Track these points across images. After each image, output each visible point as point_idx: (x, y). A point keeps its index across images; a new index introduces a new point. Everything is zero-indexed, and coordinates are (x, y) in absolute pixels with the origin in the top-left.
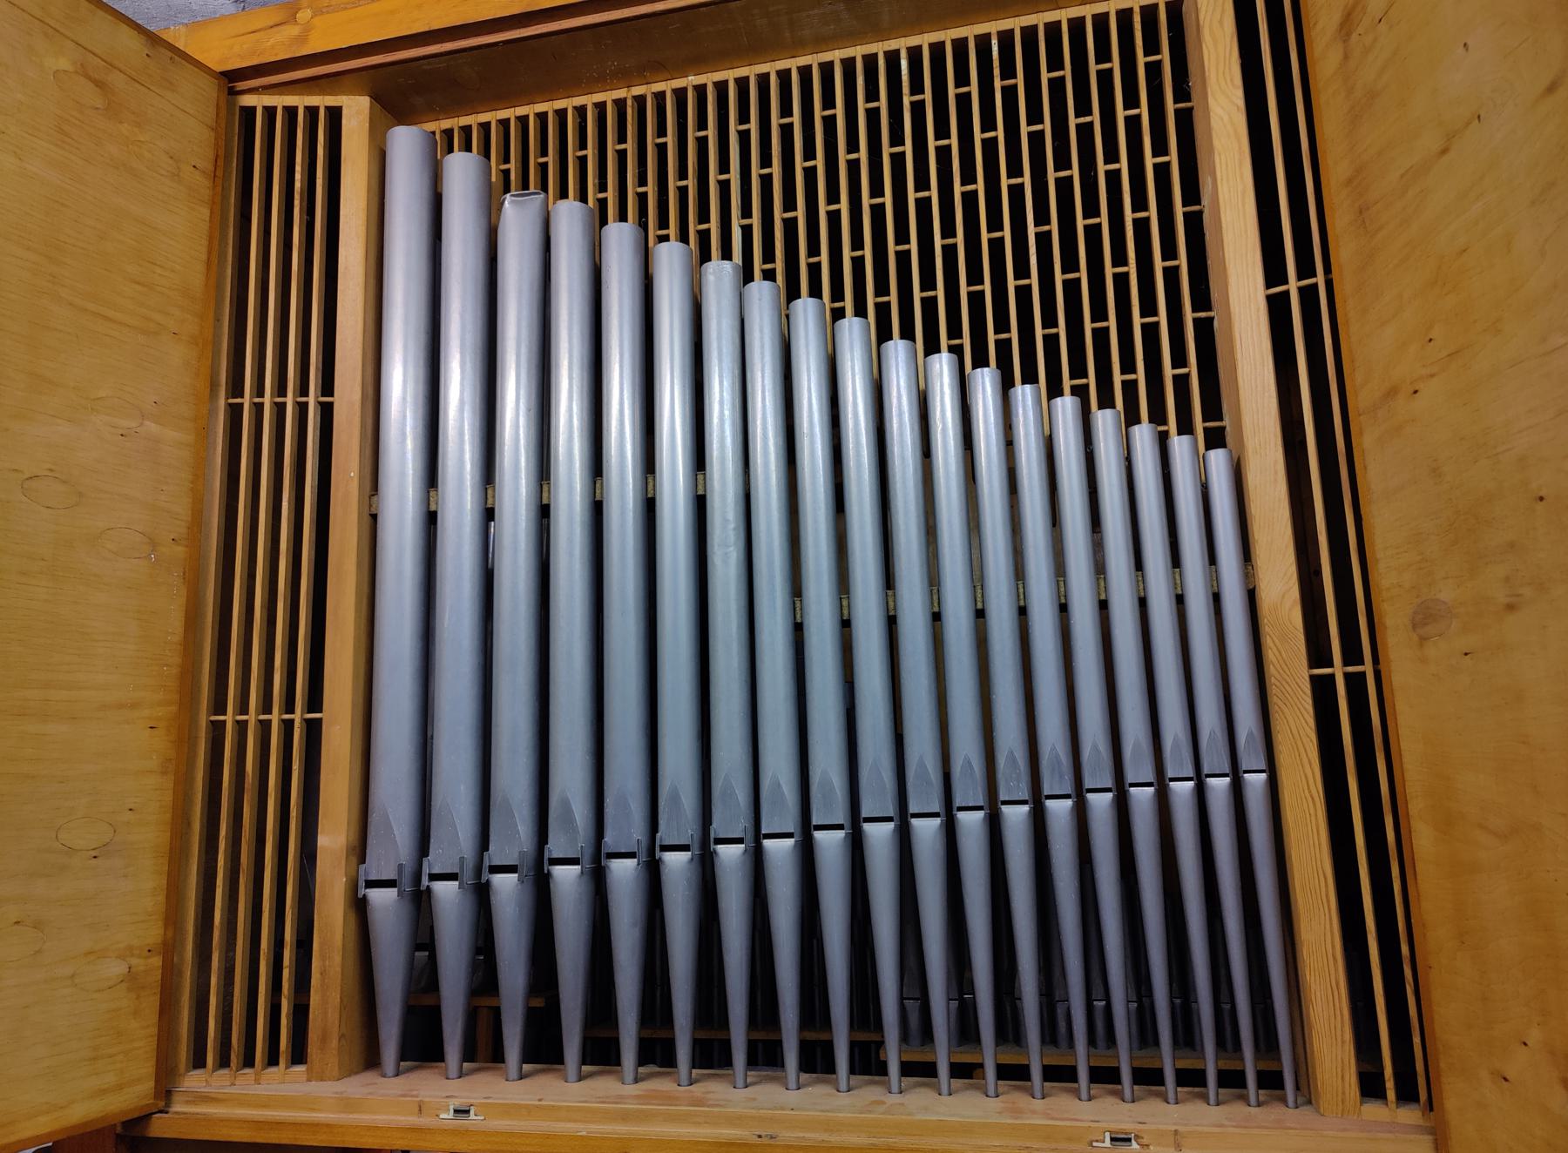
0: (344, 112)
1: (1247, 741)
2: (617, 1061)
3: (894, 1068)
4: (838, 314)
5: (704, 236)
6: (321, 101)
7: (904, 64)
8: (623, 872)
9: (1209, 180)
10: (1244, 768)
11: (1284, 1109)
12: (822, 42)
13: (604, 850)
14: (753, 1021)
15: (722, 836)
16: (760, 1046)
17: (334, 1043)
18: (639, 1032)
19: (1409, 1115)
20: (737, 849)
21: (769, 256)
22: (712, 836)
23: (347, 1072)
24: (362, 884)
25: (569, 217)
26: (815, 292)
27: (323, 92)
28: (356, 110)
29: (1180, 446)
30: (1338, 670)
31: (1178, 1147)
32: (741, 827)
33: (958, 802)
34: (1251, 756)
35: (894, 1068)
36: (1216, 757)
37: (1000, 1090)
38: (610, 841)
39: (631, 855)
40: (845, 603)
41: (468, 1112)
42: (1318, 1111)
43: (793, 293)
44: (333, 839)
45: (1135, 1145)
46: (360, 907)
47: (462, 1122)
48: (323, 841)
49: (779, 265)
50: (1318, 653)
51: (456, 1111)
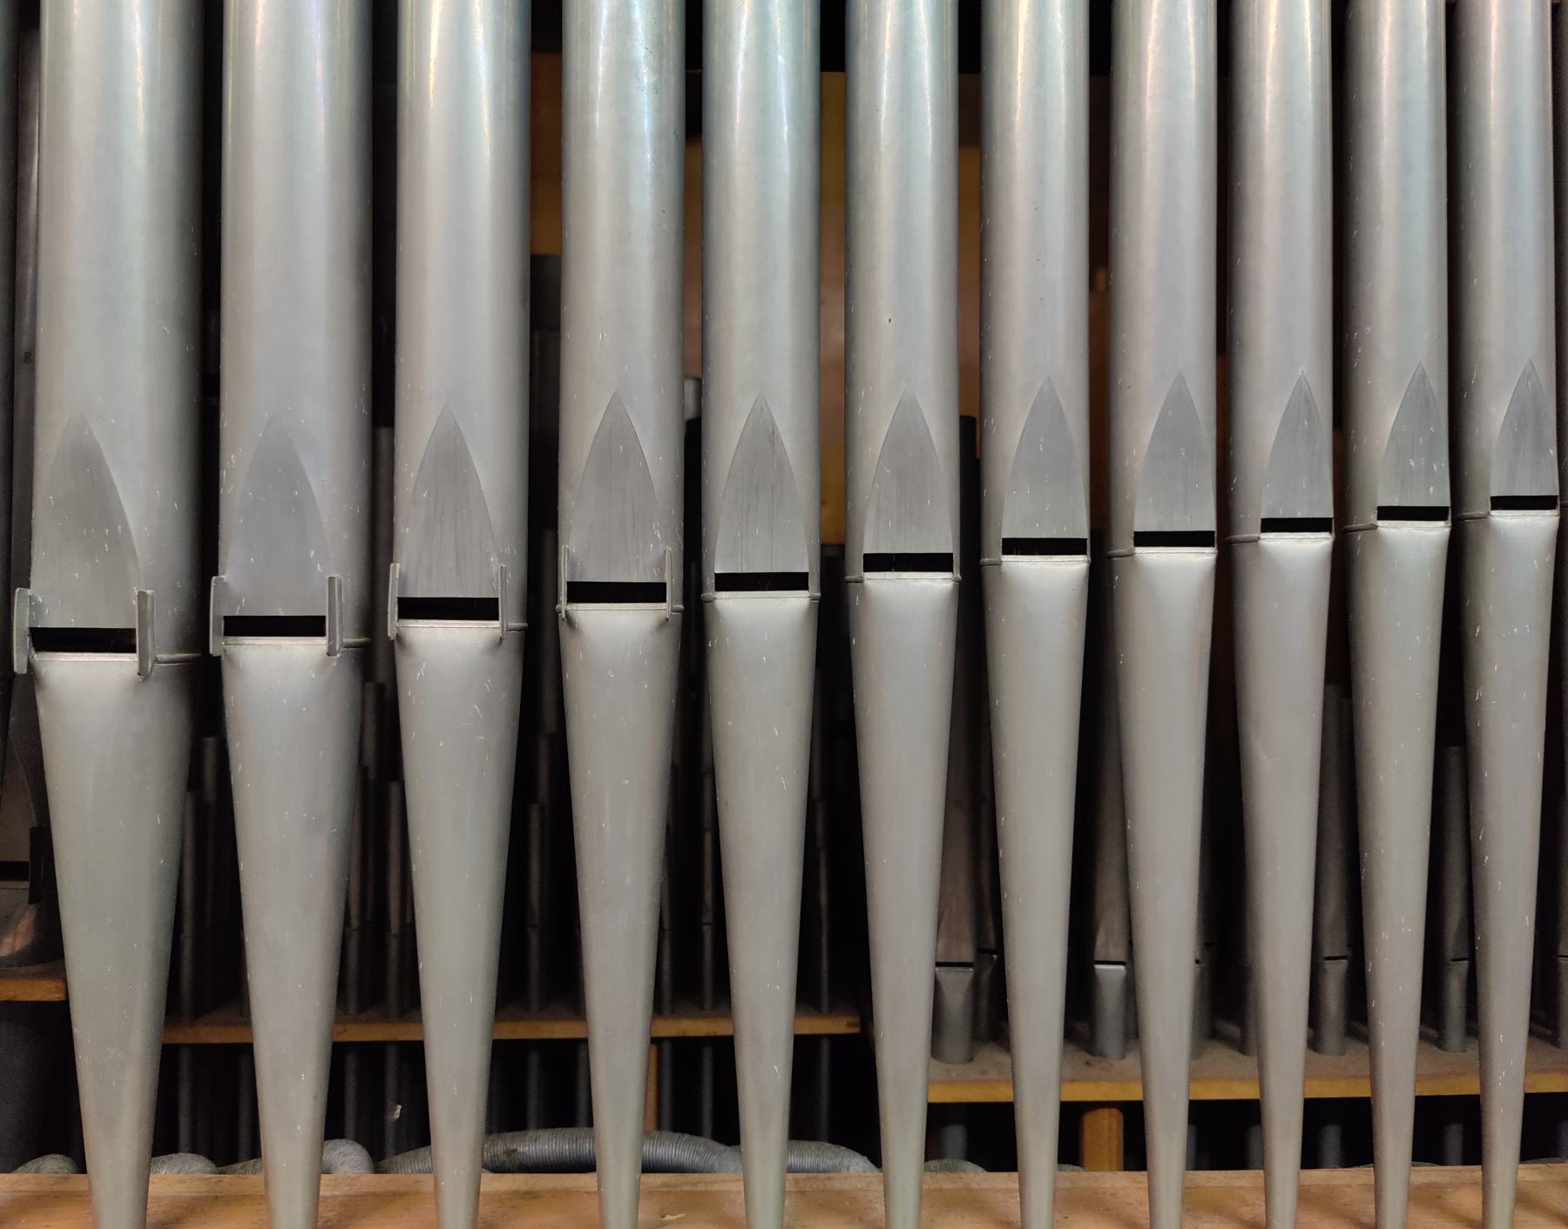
1: (1161, 432)
3: (903, 1128)
8: (452, 662)
13: (218, 610)
14: (511, 987)
16: (185, 1055)
20: (299, 655)
22: (565, 577)
32: (495, 564)
33: (721, 561)
38: (240, 583)
39: (310, 626)
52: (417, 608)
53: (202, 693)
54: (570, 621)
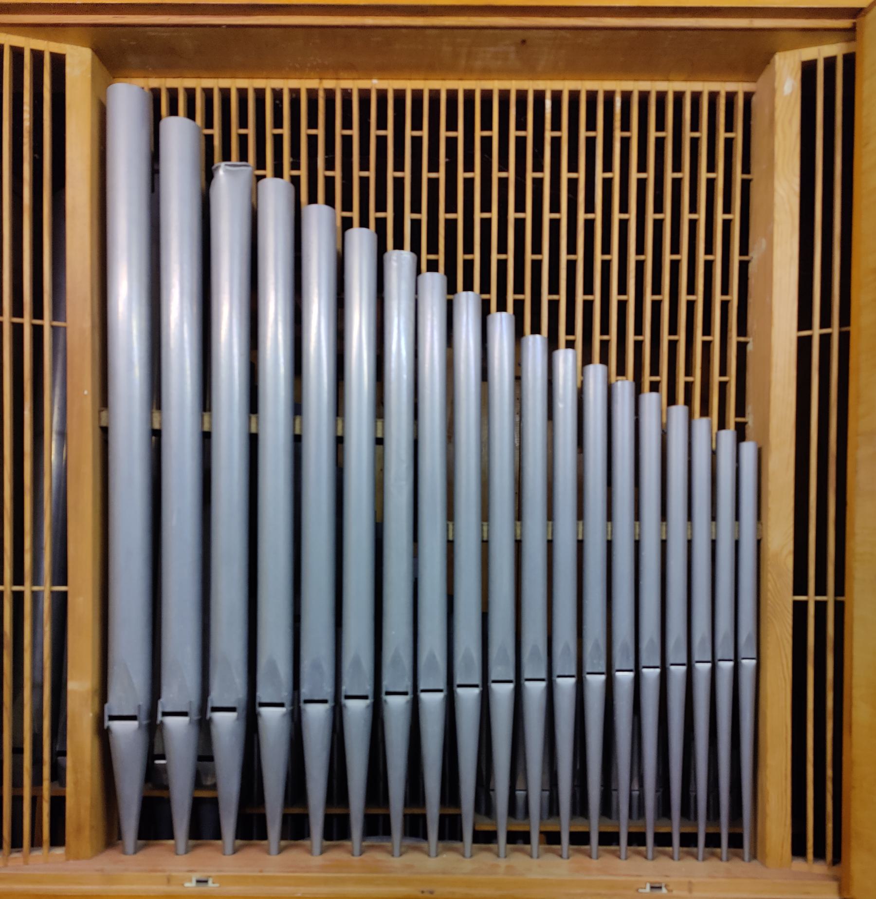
0: (68, 61)
2: (264, 836)
3: (468, 835)
4: (347, 224)
5: (381, 224)
6: (48, 47)
7: (548, 104)
9: (764, 243)
10: (743, 656)
11: (742, 863)
12: (486, 73)
14: (330, 800)
15: (391, 690)
17: (87, 832)
18: (169, 792)
19: (820, 868)
21: (570, 330)
22: (343, 694)
23: (97, 852)
24: (106, 718)
25: (275, 194)
26: (330, 201)
27: (49, 38)
28: (79, 61)
29: (701, 425)
30: (811, 598)
31: (690, 891)
33: (422, 687)
34: (747, 648)
35: (468, 835)
36: (725, 648)
37: (209, 782)
40: (485, 528)
41: (206, 882)
42: (763, 863)
43: (587, 359)
44: (80, 684)
45: (664, 890)
46: (103, 735)
47: (202, 888)
48: (73, 686)
49: (441, 257)
50: (800, 586)
51: (198, 881)
52: (215, 709)
53: (204, 727)
54: (385, 701)
